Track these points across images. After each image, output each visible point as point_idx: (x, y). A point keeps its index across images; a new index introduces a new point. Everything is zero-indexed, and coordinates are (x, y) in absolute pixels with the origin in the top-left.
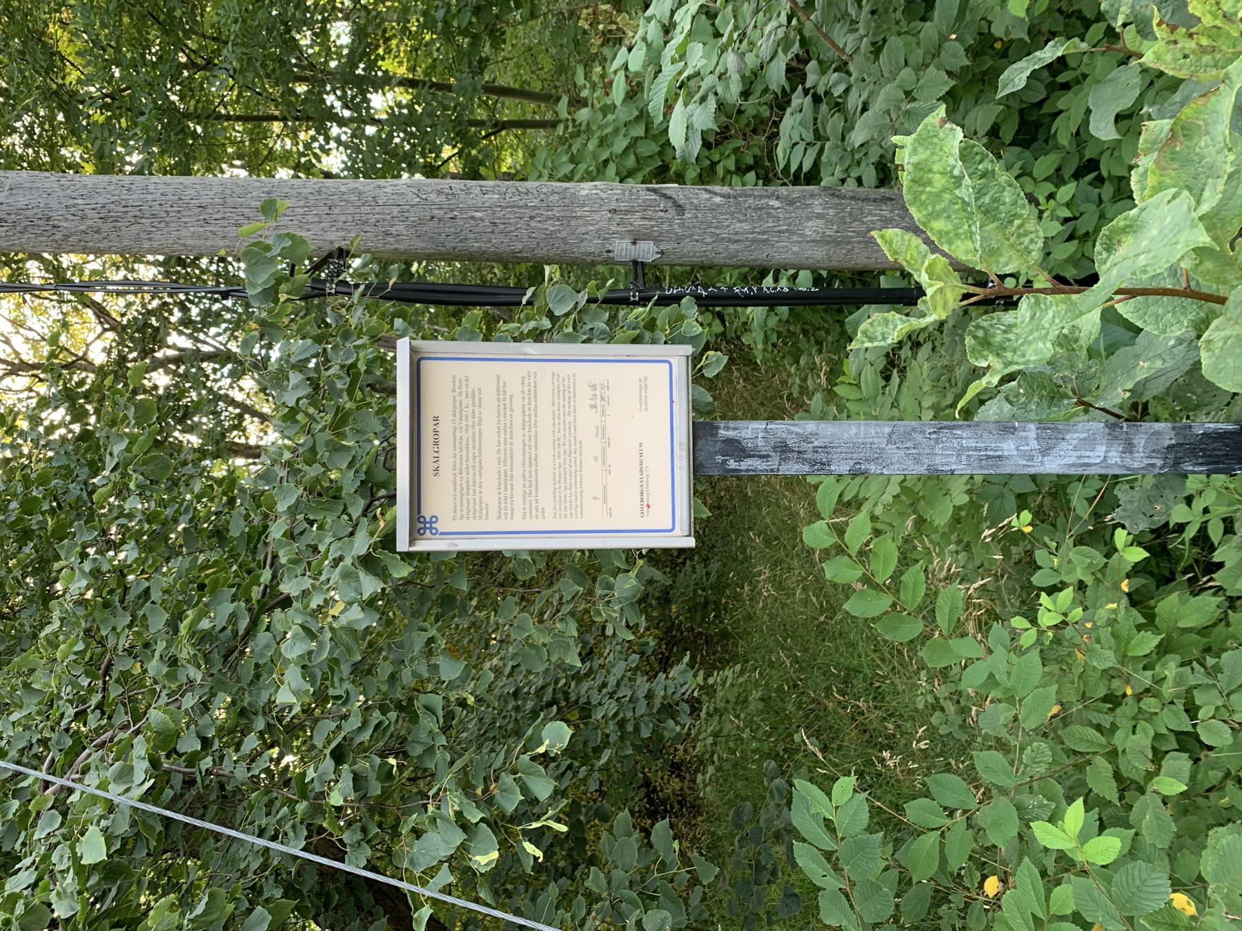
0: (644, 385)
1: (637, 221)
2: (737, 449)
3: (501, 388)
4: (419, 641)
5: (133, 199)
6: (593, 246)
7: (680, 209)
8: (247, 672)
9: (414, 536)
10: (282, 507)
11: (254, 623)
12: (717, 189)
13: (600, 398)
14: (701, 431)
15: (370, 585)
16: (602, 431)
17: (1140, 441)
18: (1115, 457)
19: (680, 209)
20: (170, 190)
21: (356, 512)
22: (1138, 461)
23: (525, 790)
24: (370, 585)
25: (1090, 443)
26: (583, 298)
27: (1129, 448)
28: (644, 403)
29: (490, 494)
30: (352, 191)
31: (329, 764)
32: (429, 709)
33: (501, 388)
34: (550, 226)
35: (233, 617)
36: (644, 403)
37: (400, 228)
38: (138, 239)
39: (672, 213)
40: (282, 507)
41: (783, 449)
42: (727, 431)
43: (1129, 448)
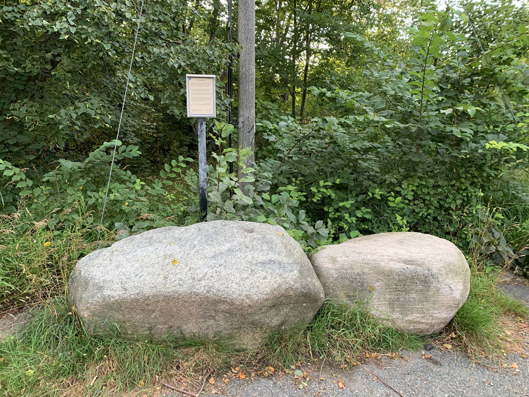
0: (210, 111)
1: (246, 123)
2: (201, 124)
3: (209, 90)
4: (165, 73)
5: (250, 9)
6: (241, 113)
7: (249, 132)
8: (154, 38)
9: (189, 77)
10: (187, 47)
11: (163, 39)
12: (254, 141)
13: (209, 104)
14: (204, 119)
15: (176, 66)
16: (204, 104)
17: (204, 183)
18: (202, 180)
19: (249, 132)
20: (252, 17)
21: (187, 62)
22: (201, 183)
23: (142, 92)
24: (176, 66)
25: (204, 176)
26: (228, 106)
27: (203, 182)
28: (208, 110)
29: (194, 88)
30: (252, 59)
31: (141, 56)
32: (151, 76)
33: (209, 90)
34: (245, 103)
35: (163, 34)
36: (208, 110)
37: (244, 70)
38: (241, 9)
39: (248, 130)
40: (187, 47)
41: (202, 131)
42: (204, 123)
43: (203, 182)
